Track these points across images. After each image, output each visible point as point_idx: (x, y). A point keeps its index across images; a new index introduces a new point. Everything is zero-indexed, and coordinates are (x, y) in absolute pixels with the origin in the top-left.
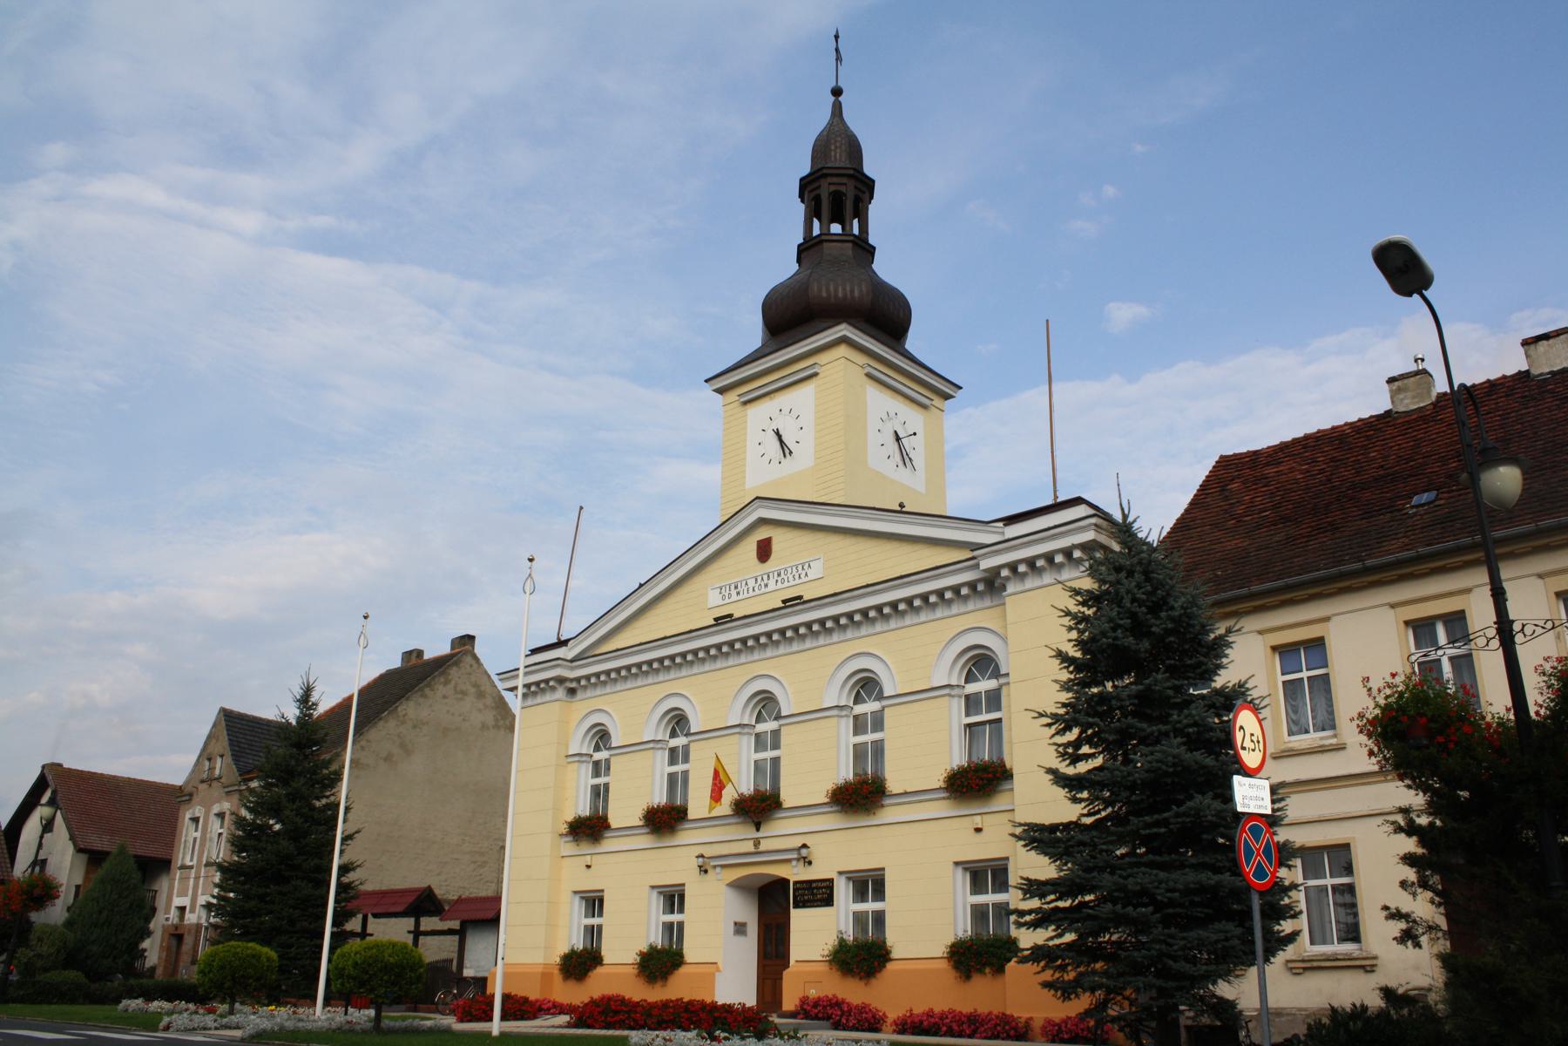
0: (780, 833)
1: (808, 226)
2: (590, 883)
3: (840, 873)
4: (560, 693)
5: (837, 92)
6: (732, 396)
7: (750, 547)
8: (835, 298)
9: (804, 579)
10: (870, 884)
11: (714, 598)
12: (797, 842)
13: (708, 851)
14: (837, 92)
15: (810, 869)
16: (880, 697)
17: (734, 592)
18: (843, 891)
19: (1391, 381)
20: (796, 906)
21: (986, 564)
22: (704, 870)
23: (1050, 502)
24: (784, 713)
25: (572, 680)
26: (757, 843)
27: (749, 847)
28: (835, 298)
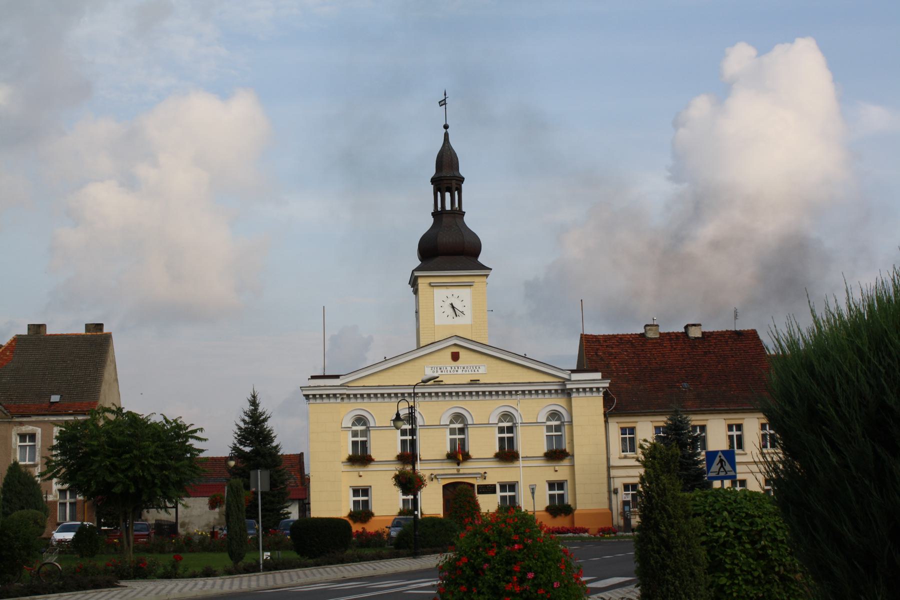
0: (467, 468)
5: (446, 127)
7: (448, 354)
8: (449, 248)
10: (512, 486)
12: (482, 471)
13: (435, 472)
14: (446, 127)
20: (479, 493)
26: (458, 470)
27: (455, 472)
28: (449, 248)
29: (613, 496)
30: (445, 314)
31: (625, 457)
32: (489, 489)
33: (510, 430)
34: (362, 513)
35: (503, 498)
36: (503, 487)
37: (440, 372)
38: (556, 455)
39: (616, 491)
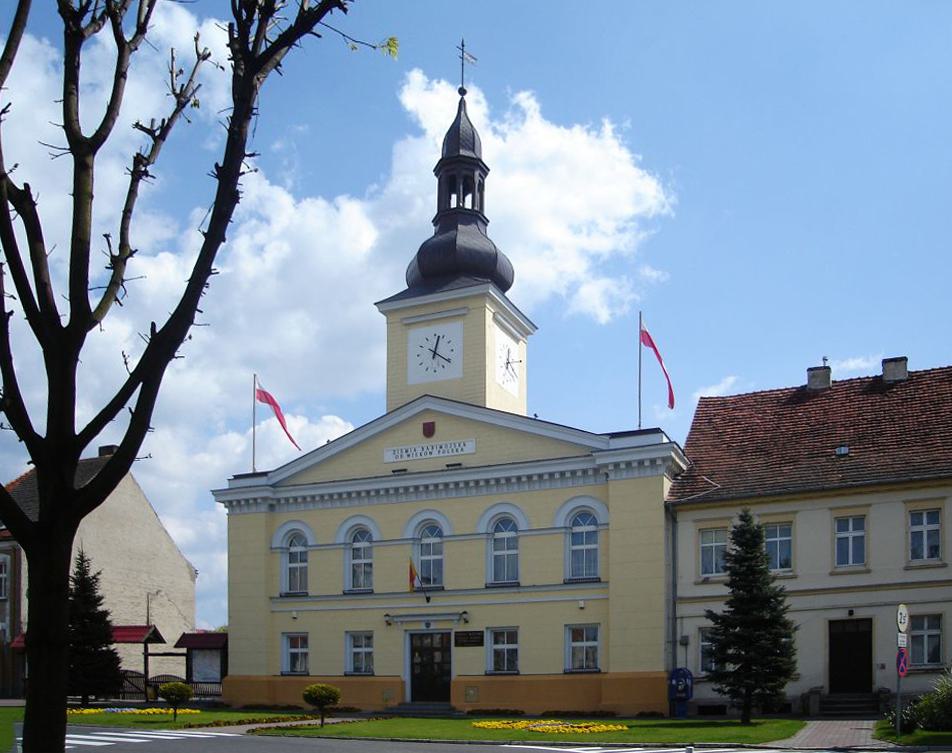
0: (440, 604)
1: (443, 200)
2: (296, 628)
3: (487, 628)
4: (264, 508)
6: (398, 317)
9: (460, 452)
11: (389, 457)
15: (467, 625)
16: (516, 531)
17: (405, 455)
18: (488, 638)
19: (810, 370)
20: (457, 645)
21: (599, 461)
22: (389, 624)
23: (637, 429)
24: (374, 539)
25: (272, 499)
29: (680, 650)
30: (424, 366)
31: (706, 581)
32: (473, 639)
33: (591, 536)
34: (362, 668)
35: (498, 654)
36: (498, 636)
37: (405, 458)
38: (584, 576)
39: (685, 642)
